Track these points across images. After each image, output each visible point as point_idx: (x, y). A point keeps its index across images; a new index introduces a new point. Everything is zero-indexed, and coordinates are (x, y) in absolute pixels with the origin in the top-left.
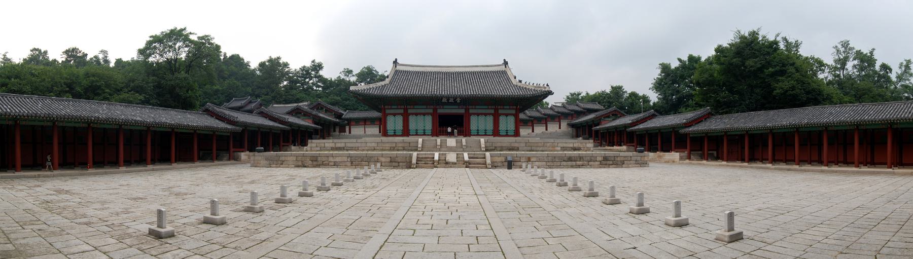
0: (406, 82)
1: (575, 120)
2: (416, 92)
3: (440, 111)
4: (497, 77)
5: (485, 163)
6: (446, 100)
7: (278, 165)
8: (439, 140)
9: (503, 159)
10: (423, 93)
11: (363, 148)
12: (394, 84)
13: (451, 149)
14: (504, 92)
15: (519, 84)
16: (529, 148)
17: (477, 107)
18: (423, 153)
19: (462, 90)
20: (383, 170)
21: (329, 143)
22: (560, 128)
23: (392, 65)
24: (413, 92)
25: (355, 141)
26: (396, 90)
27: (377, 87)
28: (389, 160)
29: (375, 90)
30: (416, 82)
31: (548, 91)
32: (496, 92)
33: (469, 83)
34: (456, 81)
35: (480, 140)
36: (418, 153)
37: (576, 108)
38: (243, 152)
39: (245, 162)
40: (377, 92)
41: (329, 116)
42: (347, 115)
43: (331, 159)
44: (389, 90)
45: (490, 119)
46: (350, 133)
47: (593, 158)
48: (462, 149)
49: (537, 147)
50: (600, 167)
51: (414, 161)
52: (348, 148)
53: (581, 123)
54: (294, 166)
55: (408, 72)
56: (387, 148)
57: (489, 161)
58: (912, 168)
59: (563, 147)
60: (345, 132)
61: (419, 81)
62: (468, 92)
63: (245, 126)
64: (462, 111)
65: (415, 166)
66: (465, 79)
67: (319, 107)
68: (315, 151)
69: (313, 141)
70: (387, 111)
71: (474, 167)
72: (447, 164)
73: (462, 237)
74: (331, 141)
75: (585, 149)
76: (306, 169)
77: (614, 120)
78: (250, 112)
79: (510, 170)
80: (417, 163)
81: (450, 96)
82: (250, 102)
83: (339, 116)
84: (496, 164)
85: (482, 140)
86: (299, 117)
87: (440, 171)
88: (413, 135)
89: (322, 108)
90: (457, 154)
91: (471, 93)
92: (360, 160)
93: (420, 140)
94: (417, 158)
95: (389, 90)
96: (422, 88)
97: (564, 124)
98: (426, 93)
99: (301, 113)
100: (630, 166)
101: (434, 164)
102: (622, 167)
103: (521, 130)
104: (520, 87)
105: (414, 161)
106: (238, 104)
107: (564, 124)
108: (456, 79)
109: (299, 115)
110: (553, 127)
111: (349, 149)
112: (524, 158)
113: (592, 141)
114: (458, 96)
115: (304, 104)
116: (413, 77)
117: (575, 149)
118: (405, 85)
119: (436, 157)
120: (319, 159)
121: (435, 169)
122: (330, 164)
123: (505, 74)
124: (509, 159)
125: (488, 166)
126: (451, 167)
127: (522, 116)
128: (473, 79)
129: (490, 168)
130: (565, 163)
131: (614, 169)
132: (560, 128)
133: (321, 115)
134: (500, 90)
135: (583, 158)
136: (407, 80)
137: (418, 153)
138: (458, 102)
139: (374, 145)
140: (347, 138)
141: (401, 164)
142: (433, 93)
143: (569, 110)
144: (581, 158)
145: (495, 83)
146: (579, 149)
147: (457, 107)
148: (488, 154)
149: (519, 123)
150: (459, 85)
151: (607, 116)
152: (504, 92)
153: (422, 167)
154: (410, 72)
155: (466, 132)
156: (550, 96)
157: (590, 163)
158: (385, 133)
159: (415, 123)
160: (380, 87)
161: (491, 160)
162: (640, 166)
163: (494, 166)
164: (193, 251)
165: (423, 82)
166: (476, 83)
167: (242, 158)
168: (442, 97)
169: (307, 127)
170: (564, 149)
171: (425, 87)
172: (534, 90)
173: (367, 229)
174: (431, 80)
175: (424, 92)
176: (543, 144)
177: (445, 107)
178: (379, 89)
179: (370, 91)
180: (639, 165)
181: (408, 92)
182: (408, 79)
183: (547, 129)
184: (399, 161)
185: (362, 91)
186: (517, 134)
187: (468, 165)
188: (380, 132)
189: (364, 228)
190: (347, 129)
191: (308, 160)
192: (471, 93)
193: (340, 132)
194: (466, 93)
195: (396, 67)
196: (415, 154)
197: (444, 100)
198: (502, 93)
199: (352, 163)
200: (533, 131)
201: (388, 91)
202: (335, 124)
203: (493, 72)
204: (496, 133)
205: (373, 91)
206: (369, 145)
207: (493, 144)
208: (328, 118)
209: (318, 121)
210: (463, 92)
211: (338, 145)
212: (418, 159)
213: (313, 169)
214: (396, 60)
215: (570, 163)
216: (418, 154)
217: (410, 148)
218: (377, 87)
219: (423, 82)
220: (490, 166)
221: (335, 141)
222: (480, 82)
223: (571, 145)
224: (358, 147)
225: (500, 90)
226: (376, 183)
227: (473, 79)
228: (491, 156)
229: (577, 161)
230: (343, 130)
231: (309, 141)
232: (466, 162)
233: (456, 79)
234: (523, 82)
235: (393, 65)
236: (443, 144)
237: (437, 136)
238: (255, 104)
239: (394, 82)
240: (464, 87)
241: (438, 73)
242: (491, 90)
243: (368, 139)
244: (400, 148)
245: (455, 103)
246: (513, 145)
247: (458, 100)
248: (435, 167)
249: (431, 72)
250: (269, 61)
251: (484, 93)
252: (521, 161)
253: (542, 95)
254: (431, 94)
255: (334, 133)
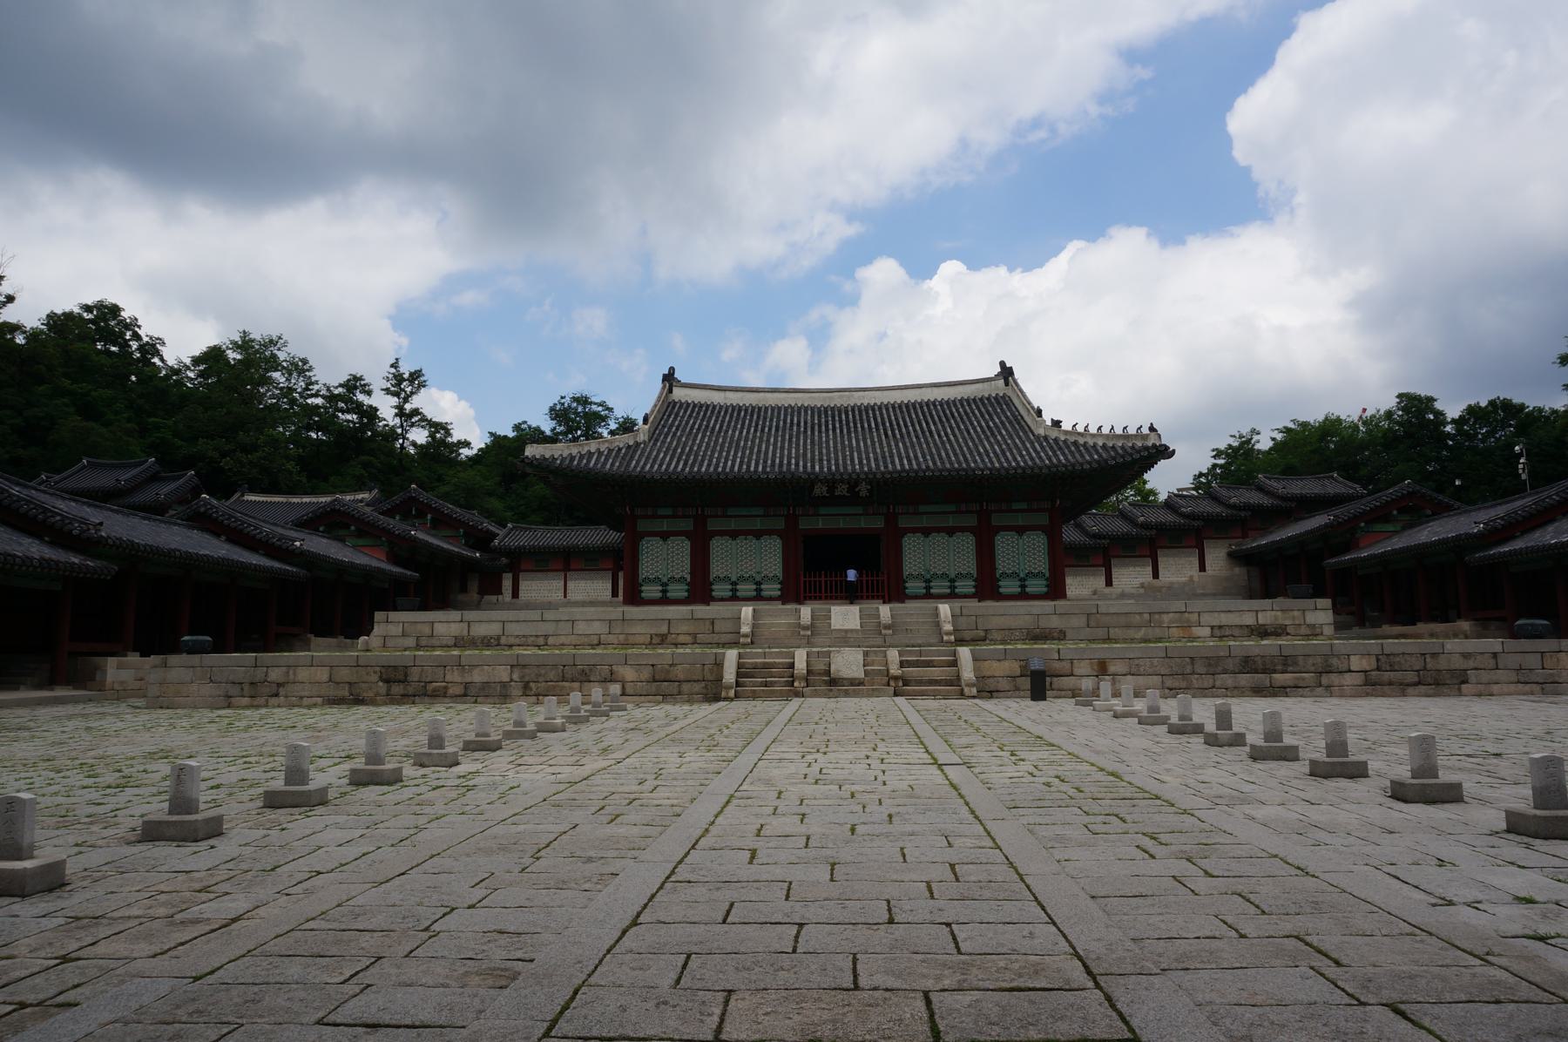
0: (703, 437)
1: (1254, 540)
2: (733, 465)
3: (804, 524)
4: (982, 416)
5: (956, 681)
6: (825, 489)
7: (261, 701)
8: (806, 612)
9: (1012, 667)
10: (756, 470)
11: (563, 639)
12: (664, 442)
13: (845, 639)
14: (1007, 459)
15: (1054, 434)
16: (1101, 633)
17: (922, 508)
18: (756, 656)
19: (876, 460)
20: (629, 706)
21: (446, 623)
22: (1202, 568)
23: (657, 386)
24: (724, 468)
25: (535, 615)
26: (671, 459)
27: (610, 451)
28: (646, 674)
29: (607, 459)
30: (733, 435)
31: (1154, 446)
32: (983, 461)
33: (894, 435)
34: (856, 431)
35: (937, 608)
36: (741, 651)
37: (1254, 498)
38: (113, 655)
39: (121, 695)
40: (612, 465)
41: (445, 538)
42: (509, 537)
43: (454, 676)
44: (648, 458)
45: (967, 543)
46: (515, 594)
47: (1335, 661)
48: (879, 641)
49: (1128, 626)
50: (1367, 695)
51: (729, 676)
52: (512, 641)
53: (1278, 547)
54: (319, 700)
55: (708, 406)
56: (640, 639)
57: (968, 673)
58: (1548, 686)
59: (1220, 627)
60: (500, 593)
61: (741, 433)
62: (893, 462)
63: (131, 556)
64: (878, 523)
65: (732, 694)
66: (884, 424)
67: (410, 509)
68: (396, 648)
69: (393, 615)
70: (642, 526)
71: (922, 694)
72: (833, 684)
73: (929, 984)
74: (455, 615)
75: (1304, 630)
76: (362, 709)
77: (1404, 529)
78: (155, 510)
79: (1042, 704)
80: (738, 684)
81: (838, 477)
82: (154, 478)
83: (481, 540)
84: (992, 685)
85: (945, 609)
86: (341, 540)
87: (815, 705)
88: (722, 600)
89: (421, 514)
90: (866, 654)
91: (902, 464)
92: (552, 675)
93: (747, 611)
94: (740, 666)
95: (648, 458)
96: (751, 453)
97: (1217, 556)
98: (764, 467)
99: (347, 527)
100: (1495, 688)
101: (791, 685)
102: (1460, 694)
103: (1069, 581)
104: (1056, 440)
105: (729, 676)
106: (105, 480)
107: (1217, 556)
108: (855, 427)
109: (342, 532)
110: (1178, 569)
111: (517, 641)
112: (1084, 663)
113: (1326, 603)
114: (863, 476)
115: (360, 496)
116: (723, 421)
117: (1262, 632)
118: (700, 446)
119: (801, 665)
120: (415, 674)
121: (796, 702)
122: (451, 691)
123: (1007, 405)
124: (1036, 665)
125: (966, 690)
126: (847, 694)
127: (1070, 534)
128: (906, 426)
129: (974, 697)
130: (1228, 680)
131: (1425, 701)
132: (1202, 568)
133: (421, 535)
134: (995, 452)
135: (1295, 663)
136: (705, 430)
137: (741, 651)
138: (864, 493)
139: (598, 628)
140: (509, 607)
141: (686, 687)
142: (785, 469)
143: (1234, 507)
144: (1287, 662)
145: (976, 431)
146: (1279, 631)
147: (860, 510)
148: (964, 653)
149: (1064, 560)
150: (865, 444)
151: (1380, 515)
152: (1007, 459)
153: (754, 696)
154: (714, 407)
155: (895, 592)
156: (1162, 464)
157: (1325, 680)
158: (634, 597)
159: (727, 558)
160: (620, 449)
161: (976, 670)
162: (1543, 692)
163: (987, 690)
164: (212, 896)
165: (754, 437)
166: (917, 437)
167: (109, 678)
168: (812, 481)
169: (368, 573)
170: (1219, 631)
171: (759, 451)
172: (1104, 446)
173: (599, 856)
174: (777, 430)
175: (756, 467)
176: (1146, 616)
177: (823, 511)
178: (617, 456)
179: (589, 461)
180: (1537, 688)
181: (709, 465)
182: (707, 426)
183: (1156, 575)
184: (681, 677)
185: (563, 459)
186: (1056, 590)
187: (900, 686)
188: (615, 594)
189: (592, 853)
190: (507, 583)
191: (375, 678)
192: (902, 464)
193: (483, 591)
194: (886, 467)
195: (670, 391)
196: (731, 656)
197: (821, 490)
198: (999, 461)
199: (526, 686)
200: (1109, 583)
201: (645, 464)
202: (469, 566)
203: (968, 400)
204: (987, 588)
205: (598, 460)
206: (581, 628)
207: (980, 620)
208: (446, 546)
209: (403, 550)
210: (877, 465)
211: (480, 630)
212: (742, 672)
213: (394, 710)
214: (672, 370)
215: (1245, 679)
216: (740, 656)
217: (716, 638)
218: (610, 451)
219: (754, 437)
220: (974, 691)
221: (471, 615)
222: (931, 432)
223: (1249, 620)
224: (546, 637)
225: (995, 452)
226: (613, 739)
227: (906, 426)
228: (975, 659)
229: (1275, 672)
230: (491, 586)
231: (379, 616)
232: (896, 678)
233: (855, 427)
234: (1066, 426)
235: (660, 385)
236: (818, 623)
237: (800, 600)
238: (173, 486)
239: (666, 438)
240: (882, 448)
241: (799, 408)
242: (964, 456)
243: (577, 612)
244: (682, 639)
245: (853, 498)
246: (1044, 623)
247: (863, 489)
248: (798, 694)
249: (779, 408)
250: (236, 346)
251: (943, 463)
252: (1076, 672)
253: (1134, 461)
254: (781, 472)
255: (461, 597)
